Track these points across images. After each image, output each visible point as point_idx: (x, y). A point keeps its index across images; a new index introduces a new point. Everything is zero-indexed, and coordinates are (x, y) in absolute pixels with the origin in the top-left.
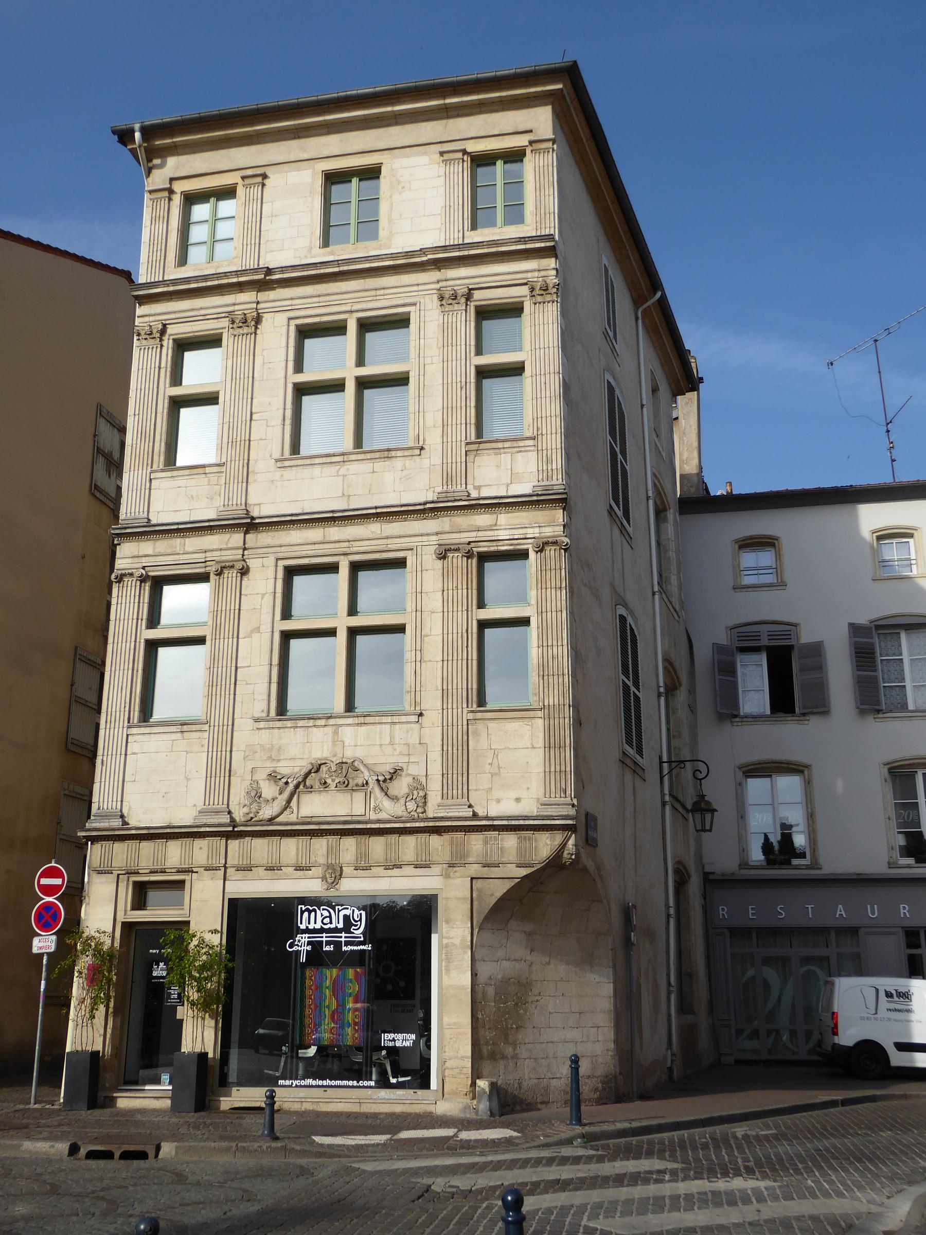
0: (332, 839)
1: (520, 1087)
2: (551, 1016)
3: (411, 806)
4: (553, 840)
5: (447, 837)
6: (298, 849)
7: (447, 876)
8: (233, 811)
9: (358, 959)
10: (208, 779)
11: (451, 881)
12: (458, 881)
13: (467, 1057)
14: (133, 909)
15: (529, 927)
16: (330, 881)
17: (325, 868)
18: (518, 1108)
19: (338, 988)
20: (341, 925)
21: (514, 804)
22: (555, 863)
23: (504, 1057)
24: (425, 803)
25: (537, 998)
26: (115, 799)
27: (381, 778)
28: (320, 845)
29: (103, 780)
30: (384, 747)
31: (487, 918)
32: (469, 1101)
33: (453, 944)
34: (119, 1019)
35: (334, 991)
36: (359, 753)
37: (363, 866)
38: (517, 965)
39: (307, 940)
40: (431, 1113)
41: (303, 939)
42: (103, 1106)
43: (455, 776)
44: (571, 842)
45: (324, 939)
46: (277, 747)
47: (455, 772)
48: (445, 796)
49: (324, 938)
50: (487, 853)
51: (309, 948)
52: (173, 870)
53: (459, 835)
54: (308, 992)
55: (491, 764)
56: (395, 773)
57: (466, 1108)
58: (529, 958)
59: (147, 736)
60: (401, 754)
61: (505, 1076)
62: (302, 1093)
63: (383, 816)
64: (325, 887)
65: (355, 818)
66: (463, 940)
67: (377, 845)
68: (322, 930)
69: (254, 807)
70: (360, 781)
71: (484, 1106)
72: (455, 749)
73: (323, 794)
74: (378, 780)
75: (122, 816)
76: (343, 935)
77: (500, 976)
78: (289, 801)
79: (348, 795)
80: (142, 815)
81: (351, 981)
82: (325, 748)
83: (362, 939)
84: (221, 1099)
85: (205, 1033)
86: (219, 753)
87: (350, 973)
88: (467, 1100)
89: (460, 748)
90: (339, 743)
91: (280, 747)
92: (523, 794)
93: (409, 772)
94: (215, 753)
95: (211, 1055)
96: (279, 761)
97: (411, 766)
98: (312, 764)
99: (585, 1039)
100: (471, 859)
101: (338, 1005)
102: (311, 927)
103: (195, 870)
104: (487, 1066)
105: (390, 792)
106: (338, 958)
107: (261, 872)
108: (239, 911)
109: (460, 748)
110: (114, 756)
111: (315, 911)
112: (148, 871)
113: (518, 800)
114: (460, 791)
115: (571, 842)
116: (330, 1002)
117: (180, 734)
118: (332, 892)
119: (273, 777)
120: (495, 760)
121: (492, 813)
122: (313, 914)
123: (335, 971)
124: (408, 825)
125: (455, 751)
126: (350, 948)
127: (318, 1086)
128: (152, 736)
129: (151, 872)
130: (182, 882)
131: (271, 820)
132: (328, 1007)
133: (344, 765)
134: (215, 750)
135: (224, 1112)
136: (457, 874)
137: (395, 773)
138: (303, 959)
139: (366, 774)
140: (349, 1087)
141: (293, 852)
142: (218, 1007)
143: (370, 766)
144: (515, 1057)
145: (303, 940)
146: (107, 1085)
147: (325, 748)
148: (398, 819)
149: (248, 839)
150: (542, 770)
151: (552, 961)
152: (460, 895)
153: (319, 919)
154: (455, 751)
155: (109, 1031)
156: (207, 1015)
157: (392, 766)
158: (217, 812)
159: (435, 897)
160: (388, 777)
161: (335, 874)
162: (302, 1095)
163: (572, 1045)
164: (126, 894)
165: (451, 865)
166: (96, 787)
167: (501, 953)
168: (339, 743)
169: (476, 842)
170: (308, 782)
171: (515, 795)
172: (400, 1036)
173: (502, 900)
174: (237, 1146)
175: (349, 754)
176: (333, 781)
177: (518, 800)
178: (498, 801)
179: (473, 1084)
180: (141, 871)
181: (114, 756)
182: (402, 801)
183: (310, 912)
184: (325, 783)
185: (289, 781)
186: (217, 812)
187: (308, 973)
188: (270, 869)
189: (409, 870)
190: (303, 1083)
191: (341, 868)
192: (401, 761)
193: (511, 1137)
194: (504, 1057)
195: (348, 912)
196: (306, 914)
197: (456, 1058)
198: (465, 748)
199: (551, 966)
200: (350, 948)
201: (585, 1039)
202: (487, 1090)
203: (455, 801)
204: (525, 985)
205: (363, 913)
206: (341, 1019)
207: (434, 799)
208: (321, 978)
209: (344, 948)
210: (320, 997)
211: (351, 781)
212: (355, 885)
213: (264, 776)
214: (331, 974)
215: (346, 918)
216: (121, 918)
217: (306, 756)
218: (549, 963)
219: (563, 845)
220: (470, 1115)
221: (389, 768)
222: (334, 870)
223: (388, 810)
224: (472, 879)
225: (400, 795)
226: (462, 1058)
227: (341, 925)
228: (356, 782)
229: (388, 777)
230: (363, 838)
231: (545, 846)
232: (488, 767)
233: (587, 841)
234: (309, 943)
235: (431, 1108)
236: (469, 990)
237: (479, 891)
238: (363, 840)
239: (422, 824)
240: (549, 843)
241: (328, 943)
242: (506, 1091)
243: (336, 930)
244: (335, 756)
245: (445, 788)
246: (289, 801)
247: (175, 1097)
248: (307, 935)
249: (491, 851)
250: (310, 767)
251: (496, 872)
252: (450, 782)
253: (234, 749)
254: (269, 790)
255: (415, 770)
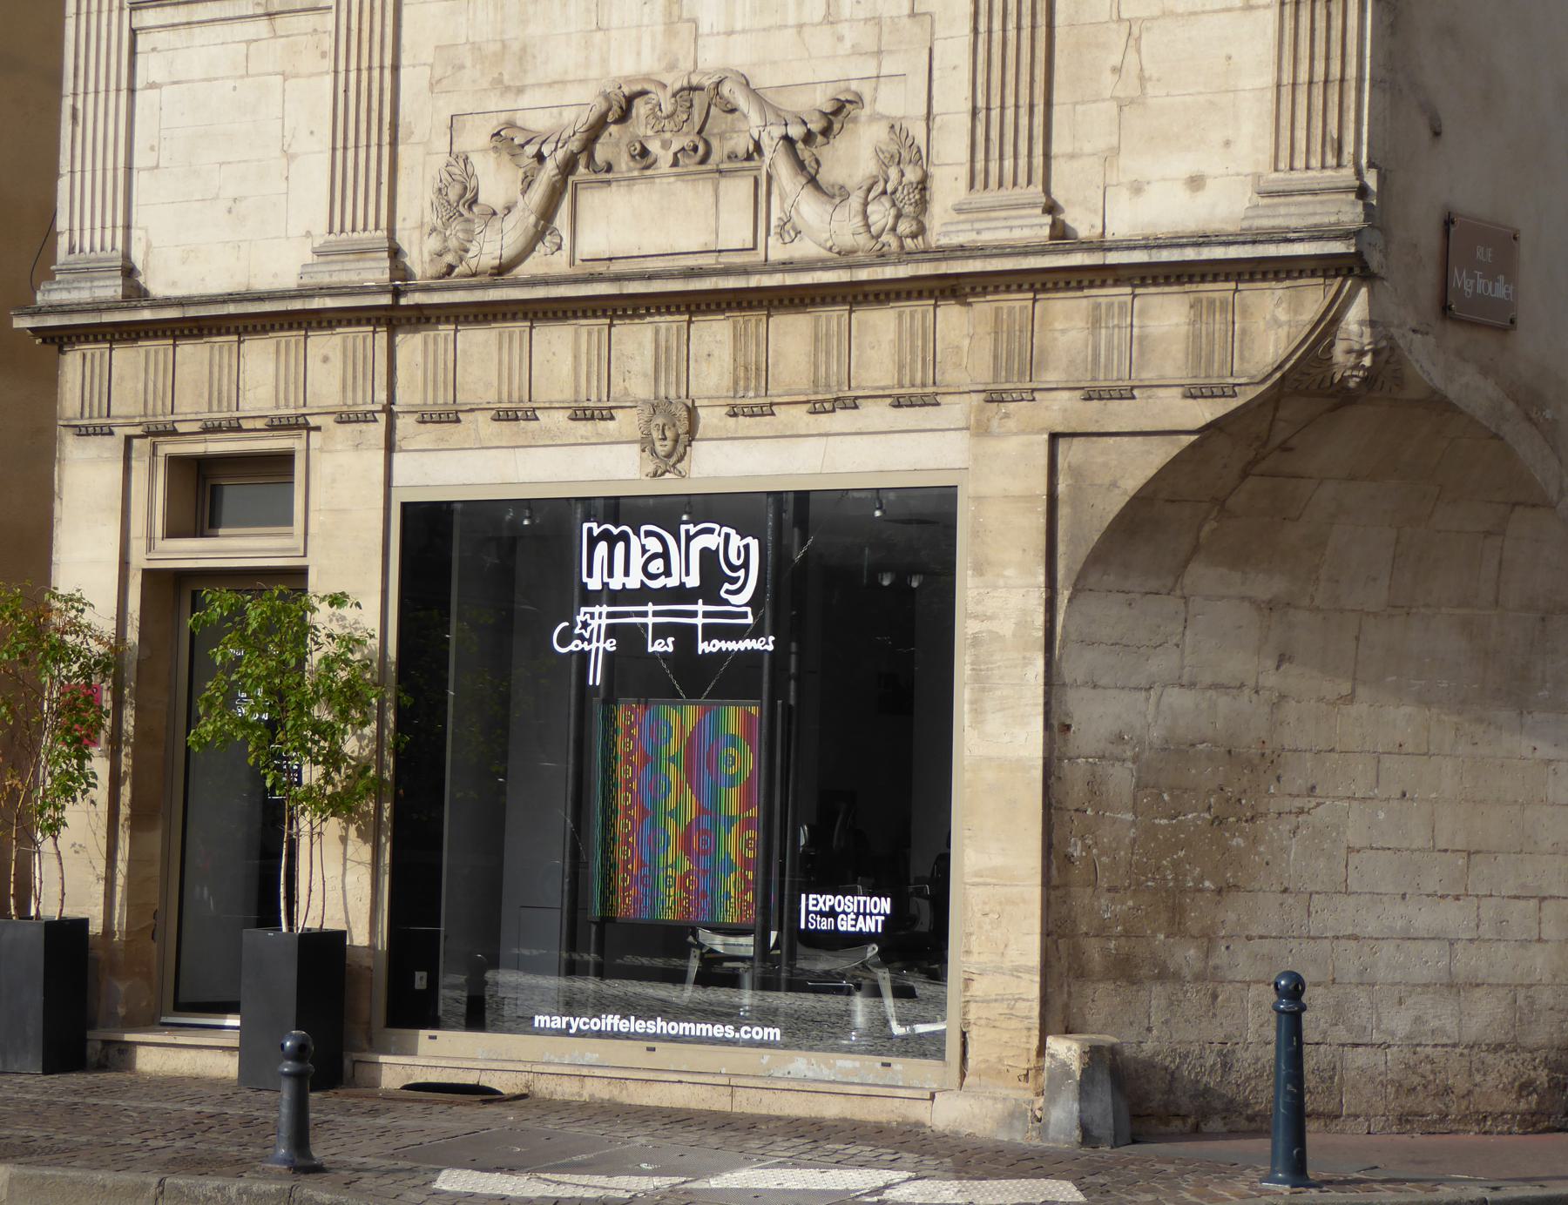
0: (669, 324)
1: (1226, 1067)
2: (1355, 859)
3: (880, 214)
4: (1296, 308)
5: (983, 308)
6: (576, 357)
7: (980, 430)
8: (405, 247)
9: (734, 678)
10: (339, 154)
11: (992, 445)
12: (1012, 445)
13: (1028, 970)
14: (172, 532)
15: (1267, 586)
16: (661, 449)
17: (648, 411)
18: (1216, 1124)
19: (699, 759)
20: (693, 581)
21: (1182, 194)
22: (1306, 379)
23: (1164, 975)
24: (923, 204)
25: (1298, 803)
26: (109, 223)
27: (796, 131)
28: (637, 341)
29: (78, 167)
30: (807, 31)
31: (1100, 557)
32: (1030, 1095)
33: (996, 637)
34: (154, 840)
35: (689, 770)
36: (739, 55)
37: (753, 406)
38: (1223, 702)
39: (605, 621)
40: (919, 1124)
41: (596, 618)
42: (102, 1067)
43: (1010, 113)
44: (1357, 312)
45: (650, 620)
46: (516, 47)
47: (1010, 101)
48: (980, 178)
49: (650, 615)
50: (1096, 356)
51: (610, 645)
52: (260, 424)
53: (1016, 303)
54: (623, 772)
55: (1117, 70)
56: (839, 114)
57: (1014, 1115)
58: (1271, 680)
59: (183, 32)
60: (857, 52)
61: (1156, 1028)
62: (592, 1051)
63: (805, 249)
64: (651, 468)
65: (726, 259)
66: (1022, 624)
67: (791, 336)
68: (642, 595)
69: (456, 231)
70: (742, 144)
71: (1064, 1114)
72: (1011, 25)
73: (640, 187)
74: (786, 138)
75: (129, 272)
76: (700, 607)
77: (1155, 734)
78: (547, 214)
79: (705, 189)
80: (180, 269)
81: (733, 741)
82: (647, 40)
83: (750, 620)
84: (382, 1059)
85: (348, 879)
86: (365, 75)
87: (733, 717)
88: (1024, 1094)
89: (1026, 22)
90: (685, 29)
91: (524, 50)
92: (1210, 163)
93: (881, 107)
94: (353, 76)
95: (96, 928)
96: (520, 91)
97: (885, 90)
98: (607, 97)
99: (1487, 931)
100: (1051, 377)
101: (701, 810)
102: (616, 584)
103: (313, 421)
104: (1101, 1000)
105: (824, 177)
106: (691, 675)
107: (482, 423)
108: (432, 540)
109: (1026, 22)
110: (102, 96)
111: (624, 537)
112: (195, 427)
113: (1196, 182)
114: (1023, 162)
115: (1357, 312)
116: (681, 802)
117: (263, 24)
118: (670, 485)
119: (505, 140)
120: (1132, 57)
121: (1119, 229)
122: (620, 546)
123: (691, 713)
124: (863, 275)
125: (1012, 34)
126: (717, 645)
127: (628, 1036)
128: (197, 30)
129: (206, 430)
130: (281, 464)
131: (502, 270)
132: (674, 814)
133: (696, 96)
134: (353, 65)
135: (390, 1097)
136: (1011, 424)
137: (839, 114)
138: (596, 676)
139: (755, 119)
140: (713, 1041)
141: (565, 366)
142: (379, 809)
143: (770, 96)
144: (1209, 977)
145: (594, 624)
146: (121, 1011)
147: (647, 40)
148: (846, 258)
149: (446, 330)
150: (1269, 79)
151: (1362, 691)
152: (1017, 487)
153: (637, 561)
154: (1012, 34)
155: (122, 867)
156: (352, 829)
157: (831, 91)
158: (362, 252)
159: (947, 496)
160: (816, 126)
161: (677, 429)
162: (592, 1057)
163: (1432, 949)
164: (151, 494)
165: (995, 397)
166: (63, 184)
167: (1161, 664)
168: (685, 29)
169: (1066, 322)
170: (601, 153)
171: (1183, 166)
172: (848, 903)
173: (1143, 500)
174: (161, 1183)
175: (712, 58)
176: (666, 145)
177: (1196, 182)
178: (1137, 189)
179: (1041, 1050)
180: (181, 428)
181: (102, 96)
182: (855, 202)
183: (612, 540)
184: (644, 152)
185: (546, 150)
186: (362, 252)
187: (623, 716)
188: (506, 416)
189: (876, 414)
190: (595, 1024)
191: (692, 412)
192: (847, 71)
193: (673, 1185)
194: (1164, 975)
195: (712, 541)
196: (602, 548)
197: (998, 970)
198: (1041, 20)
199: (1359, 708)
200: (717, 645)
201: (1487, 931)
202: (1076, 1066)
203: (1009, 194)
204: (1266, 763)
205: (754, 545)
206: (710, 850)
207: (949, 187)
208: (654, 732)
209: (703, 647)
210: (654, 787)
211: (715, 143)
212: (728, 461)
213: (483, 139)
214: (682, 718)
215: (708, 556)
216: (140, 560)
217: (594, 72)
218: (1350, 698)
219: (1329, 325)
220: (1022, 1136)
221: (821, 100)
222: (672, 417)
223: (817, 231)
224: (1054, 437)
225: (850, 184)
226: (1016, 971)
227: (693, 581)
228: (729, 146)
229: (816, 126)
230: (753, 320)
231: (1273, 325)
232: (1108, 78)
233: (1445, 309)
234: (612, 631)
235: (919, 1112)
236: (1038, 774)
237: (1076, 473)
238: (758, 322)
239: (903, 271)
240: (1283, 316)
241: (661, 631)
242: (1173, 1076)
243: (682, 594)
244: (672, 67)
245: (980, 155)
246: (547, 214)
247: (247, 1052)
248: (605, 609)
249: (1109, 349)
250: (600, 106)
251: (1121, 415)
252: (994, 134)
253: (405, 60)
254: (496, 182)
255: (897, 101)
